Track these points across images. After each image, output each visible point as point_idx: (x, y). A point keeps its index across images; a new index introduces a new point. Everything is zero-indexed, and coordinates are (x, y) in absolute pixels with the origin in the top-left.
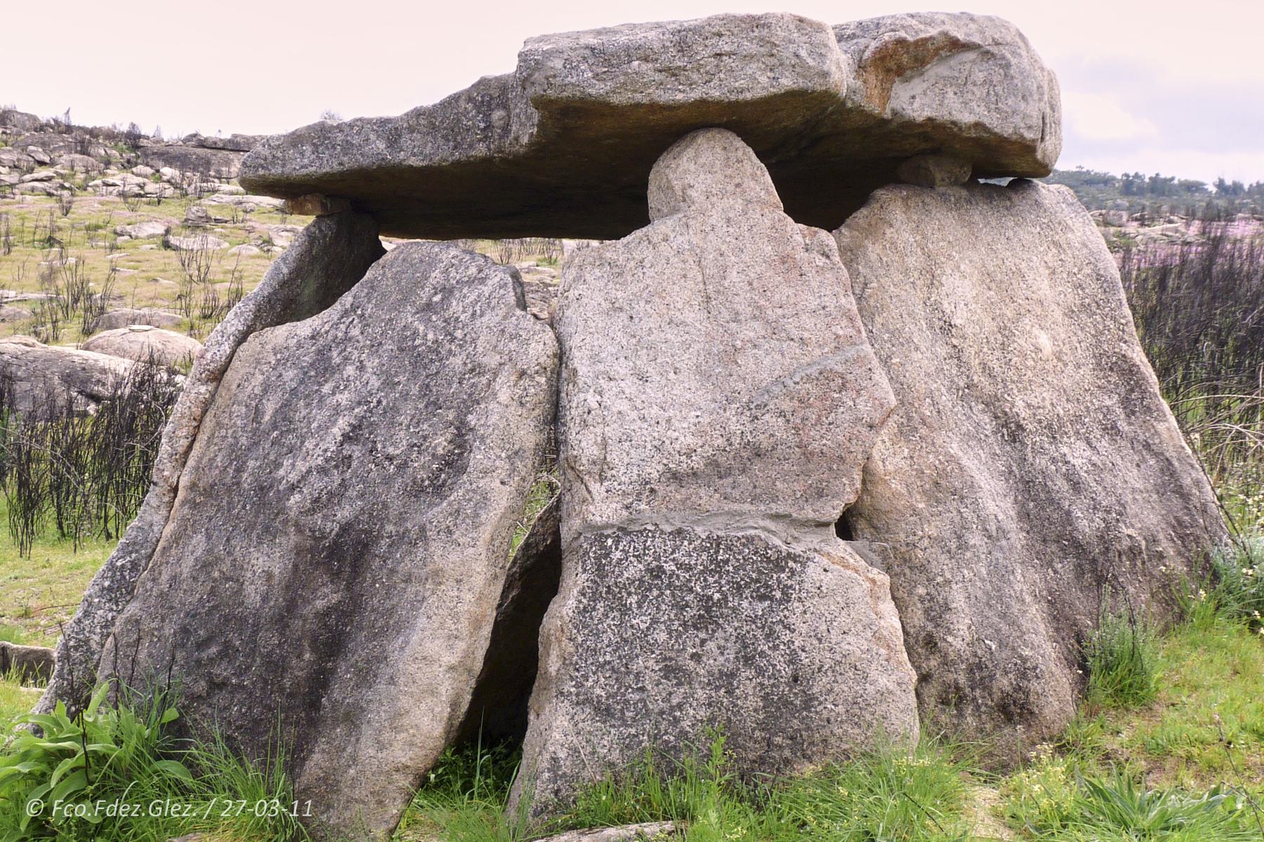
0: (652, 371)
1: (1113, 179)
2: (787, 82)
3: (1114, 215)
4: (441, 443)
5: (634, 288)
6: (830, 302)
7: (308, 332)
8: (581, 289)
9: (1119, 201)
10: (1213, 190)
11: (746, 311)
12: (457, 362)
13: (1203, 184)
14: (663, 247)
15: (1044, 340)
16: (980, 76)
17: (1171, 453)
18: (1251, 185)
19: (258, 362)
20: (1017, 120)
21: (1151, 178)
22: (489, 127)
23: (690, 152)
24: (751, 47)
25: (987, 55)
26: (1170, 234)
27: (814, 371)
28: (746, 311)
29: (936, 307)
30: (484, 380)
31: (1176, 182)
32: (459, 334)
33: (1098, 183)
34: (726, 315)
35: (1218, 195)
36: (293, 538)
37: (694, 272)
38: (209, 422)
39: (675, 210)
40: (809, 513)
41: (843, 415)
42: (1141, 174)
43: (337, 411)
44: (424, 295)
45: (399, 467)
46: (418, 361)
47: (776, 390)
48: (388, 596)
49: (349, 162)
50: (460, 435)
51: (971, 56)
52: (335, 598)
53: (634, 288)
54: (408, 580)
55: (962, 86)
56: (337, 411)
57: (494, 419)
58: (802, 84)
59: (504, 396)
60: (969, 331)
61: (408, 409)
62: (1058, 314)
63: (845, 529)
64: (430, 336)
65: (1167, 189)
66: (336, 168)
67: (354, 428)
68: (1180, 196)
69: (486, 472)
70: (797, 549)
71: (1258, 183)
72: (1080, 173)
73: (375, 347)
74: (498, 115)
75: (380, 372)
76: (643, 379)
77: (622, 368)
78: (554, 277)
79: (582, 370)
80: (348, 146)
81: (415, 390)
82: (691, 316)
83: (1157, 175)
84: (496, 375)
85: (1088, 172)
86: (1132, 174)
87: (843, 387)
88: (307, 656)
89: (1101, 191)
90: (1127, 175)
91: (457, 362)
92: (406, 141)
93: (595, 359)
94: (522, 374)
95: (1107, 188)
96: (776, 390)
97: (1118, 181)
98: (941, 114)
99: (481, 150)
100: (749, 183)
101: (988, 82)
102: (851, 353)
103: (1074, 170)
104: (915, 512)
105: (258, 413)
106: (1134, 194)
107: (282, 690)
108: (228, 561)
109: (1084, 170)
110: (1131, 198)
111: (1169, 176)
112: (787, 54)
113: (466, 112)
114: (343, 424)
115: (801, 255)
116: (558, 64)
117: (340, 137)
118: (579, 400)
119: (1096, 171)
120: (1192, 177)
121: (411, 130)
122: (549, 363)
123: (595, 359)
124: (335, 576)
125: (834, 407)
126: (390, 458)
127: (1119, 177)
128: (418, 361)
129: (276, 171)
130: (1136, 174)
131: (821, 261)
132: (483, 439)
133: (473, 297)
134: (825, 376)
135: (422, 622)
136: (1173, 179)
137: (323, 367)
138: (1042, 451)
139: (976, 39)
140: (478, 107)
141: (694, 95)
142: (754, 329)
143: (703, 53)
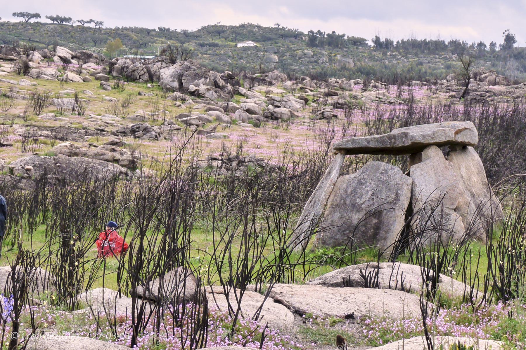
0: (428, 185)
1: (301, 34)
2: (447, 139)
3: (346, 83)
4: (393, 196)
5: (424, 171)
6: (453, 174)
7: (354, 177)
8: (416, 171)
9: (306, 51)
10: (371, 44)
11: (441, 175)
12: (393, 183)
13: (365, 40)
14: (428, 165)
15: (475, 179)
16: (469, 133)
17: (495, 201)
18: (398, 42)
19: (344, 182)
20: (474, 141)
21: (328, 35)
22: (391, 142)
23: (430, 149)
24: (443, 134)
25: (470, 130)
26: (381, 97)
27: (451, 185)
28: (441, 175)
29: (460, 173)
30: (400, 186)
31: (346, 38)
32: (392, 178)
33: (291, 37)
34: (438, 176)
35: (375, 49)
36: (364, 212)
37: (433, 169)
38: (333, 193)
39: (428, 159)
40: (451, 207)
41: (455, 192)
42: (322, 31)
43: (368, 191)
44: (380, 171)
45: (385, 200)
46: (383, 183)
47: (446, 188)
48: (388, 220)
49: (359, 146)
50: (397, 194)
51: (468, 130)
52: (377, 221)
53: (424, 171)
54: (391, 217)
55: (466, 135)
56: (368, 191)
57: (404, 192)
58: (450, 139)
59: (405, 188)
60: (465, 177)
61: (384, 191)
62: (476, 174)
63: (455, 210)
64: (385, 178)
65: (340, 42)
66: (356, 147)
67: (373, 193)
68: (349, 49)
69: (404, 200)
70: (450, 213)
71: (402, 40)
72: (278, 29)
73: (372, 180)
74: (393, 140)
75: (375, 184)
76: (426, 186)
77: (423, 184)
78: (71, 123)
79: (417, 184)
80: (359, 143)
81: (385, 187)
82: (433, 176)
83: (334, 32)
84: (402, 185)
85: (289, 30)
86: (315, 31)
87: (455, 188)
88: (372, 230)
89: (293, 43)
90: (312, 32)
91: (393, 183)
92: (371, 142)
93: (419, 183)
94: (408, 185)
95: (296, 41)
96: (446, 188)
97: (305, 36)
98: (463, 140)
99: (389, 146)
100: (439, 154)
101: (470, 135)
102: (456, 182)
103: (274, 26)
104: (464, 208)
105: (346, 191)
106: (317, 46)
107: (367, 236)
108: (348, 217)
109: (280, 27)
110: (314, 49)
111: (341, 34)
112: (448, 135)
113: (386, 139)
114: (370, 193)
115: (448, 166)
116: (417, 137)
117: (357, 141)
118: (417, 190)
119: (289, 28)
120: (357, 35)
121: (372, 141)
122: (411, 183)
123: (419, 183)
124: (375, 218)
125: (454, 191)
126: (383, 199)
127: (306, 33)
128: (383, 183)
129: (344, 147)
130: (319, 31)
131: (451, 167)
132: (402, 195)
133: (393, 172)
134: (452, 186)
135: (396, 223)
136: (344, 35)
137: (360, 183)
138: (477, 199)
139: (469, 128)
140: (389, 139)
141: (435, 141)
142: (441, 178)
143: (436, 135)
